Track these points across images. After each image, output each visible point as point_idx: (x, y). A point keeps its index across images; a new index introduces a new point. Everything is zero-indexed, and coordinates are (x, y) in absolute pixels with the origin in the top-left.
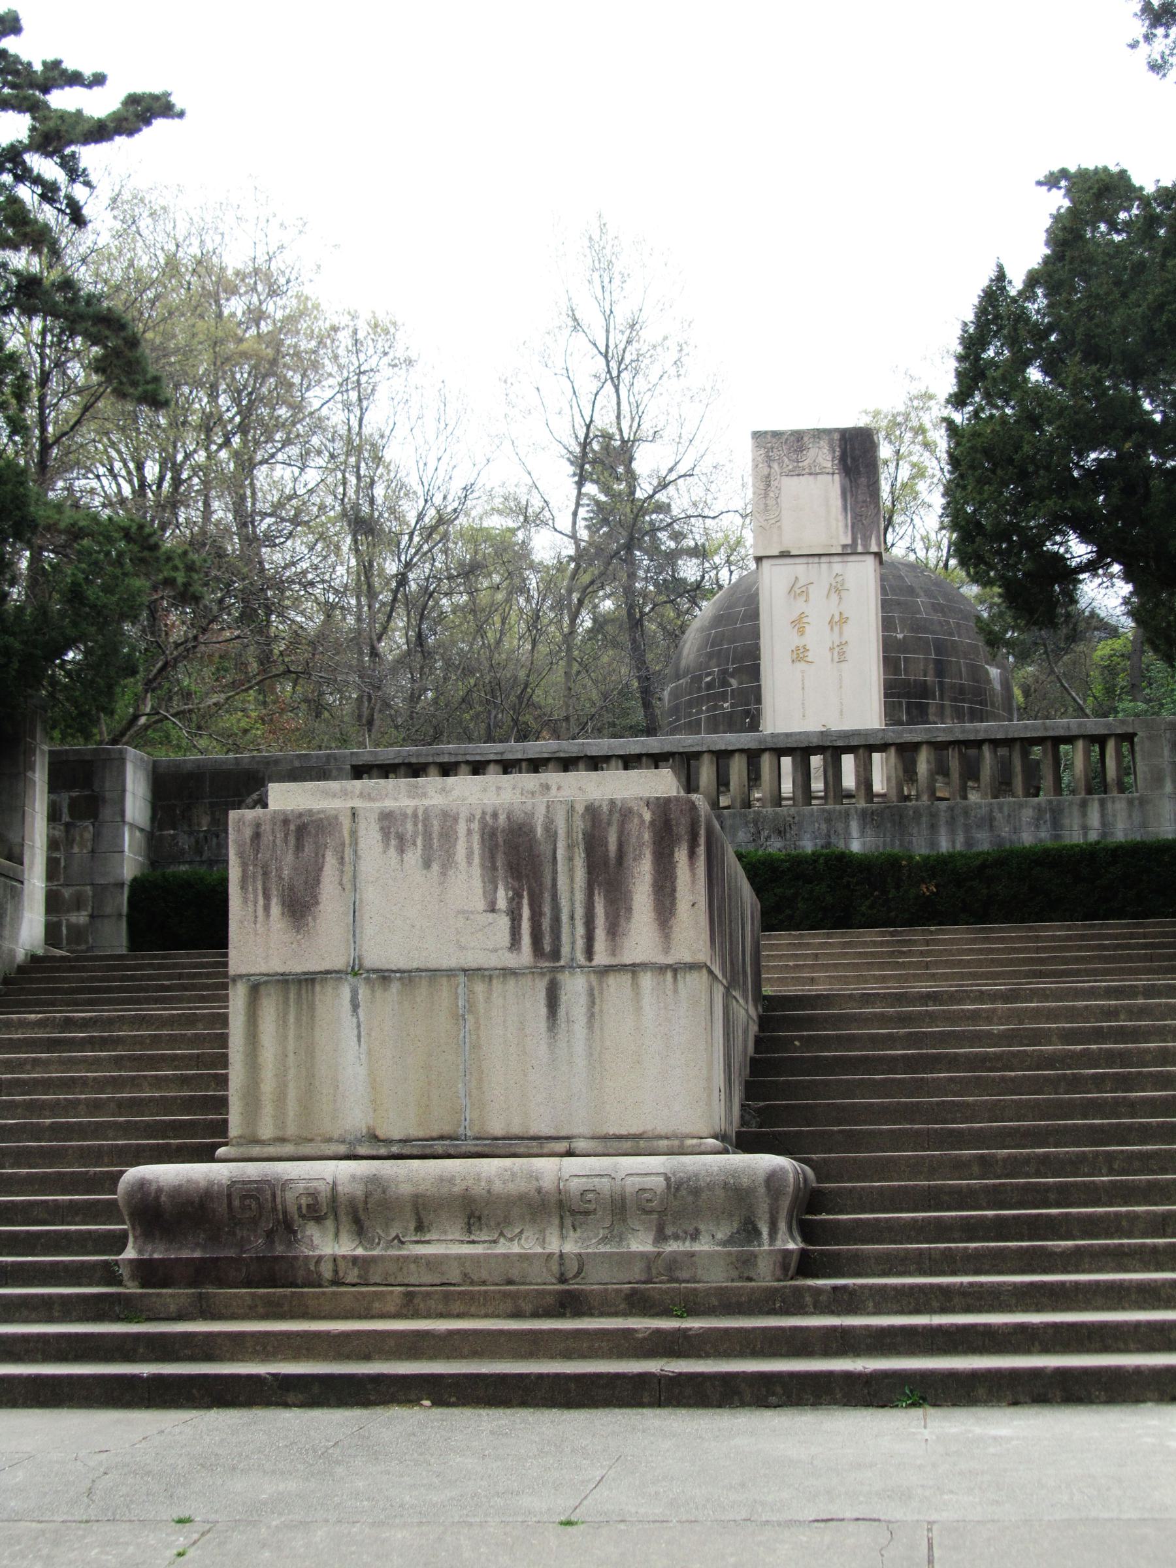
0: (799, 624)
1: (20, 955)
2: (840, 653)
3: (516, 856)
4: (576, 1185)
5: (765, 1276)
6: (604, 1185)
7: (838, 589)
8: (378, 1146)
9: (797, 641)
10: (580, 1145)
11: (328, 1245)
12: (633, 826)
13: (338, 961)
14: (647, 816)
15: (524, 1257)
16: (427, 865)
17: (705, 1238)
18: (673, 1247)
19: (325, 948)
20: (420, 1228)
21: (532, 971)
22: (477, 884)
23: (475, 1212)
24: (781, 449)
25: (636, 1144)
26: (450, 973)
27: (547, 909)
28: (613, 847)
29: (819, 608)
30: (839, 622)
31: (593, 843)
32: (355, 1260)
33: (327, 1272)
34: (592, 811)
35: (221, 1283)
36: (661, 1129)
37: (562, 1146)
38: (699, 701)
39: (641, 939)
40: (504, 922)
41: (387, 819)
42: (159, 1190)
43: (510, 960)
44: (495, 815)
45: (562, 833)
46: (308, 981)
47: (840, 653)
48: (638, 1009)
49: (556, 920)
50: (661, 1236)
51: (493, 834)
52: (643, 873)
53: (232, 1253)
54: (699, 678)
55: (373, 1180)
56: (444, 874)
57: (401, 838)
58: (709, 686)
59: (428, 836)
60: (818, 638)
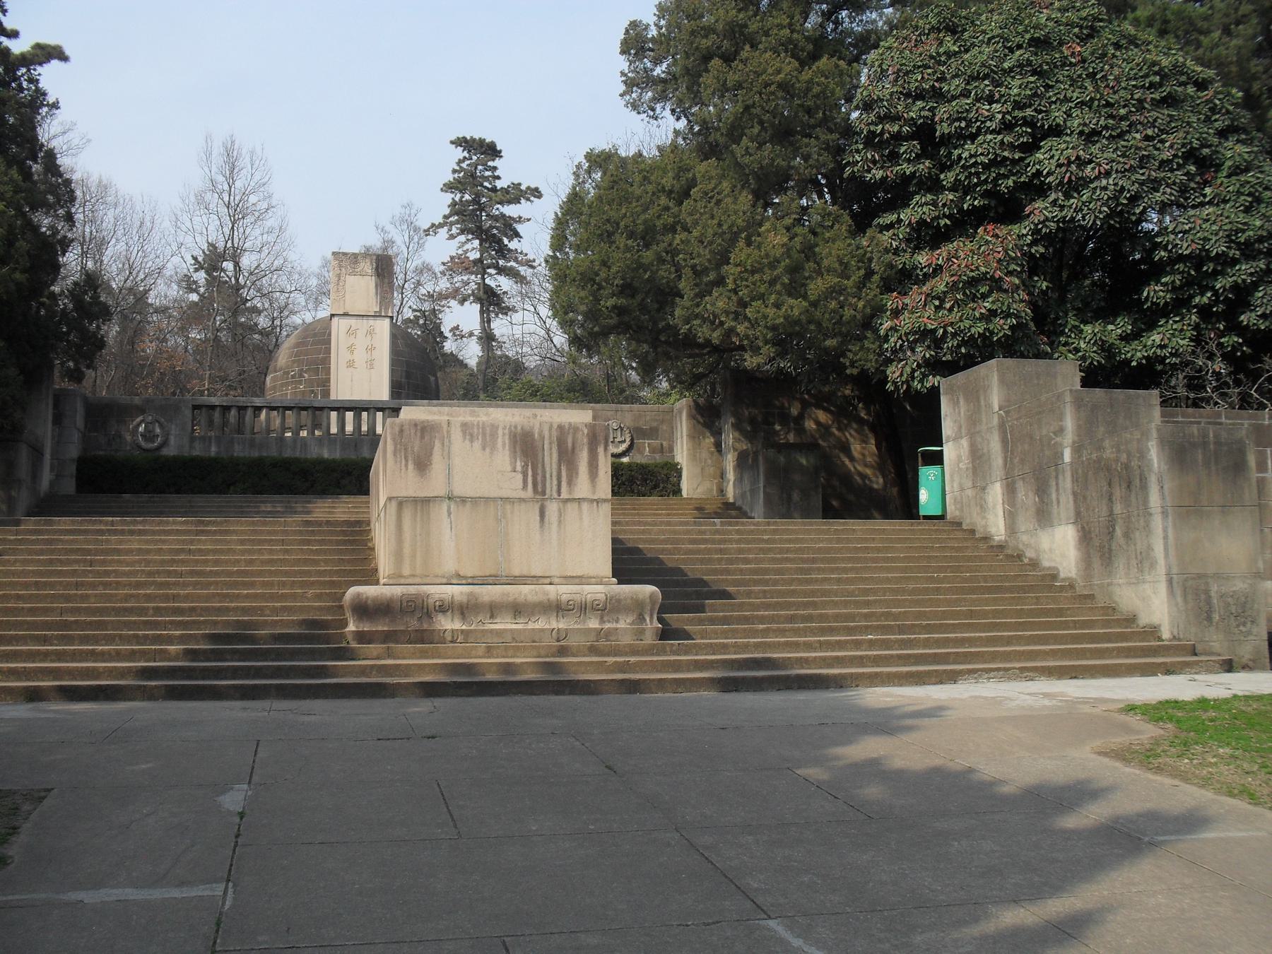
0: (351, 349)
1: (42, 495)
2: (371, 364)
3: (525, 446)
4: (564, 598)
5: (649, 639)
6: (577, 598)
7: (371, 332)
8: (459, 579)
9: (350, 357)
10: (556, 580)
11: (448, 624)
12: (579, 435)
13: (442, 493)
14: (586, 431)
15: (542, 630)
16: (484, 449)
17: (622, 622)
18: (607, 626)
19: (435, 485)
20: (492, 617)
21: (532, 500)
22: (507, 459)
23: (518, 609)
24: (346, 260)
25: (581, 580)
26: (494, 499)
27: (540, 472)
28: (570, 445)
29: (361, 342)
30: (370, 349)
31: (561, 443)
32: (462, 631)
33: (448, 637)
34: (560, 427)
35: (397, 643)
36: (591, 574)
37: (548, 581)
38: (287, 384)
39: (583, 487)
40: (520, 476)
41: (465, 427)
42: (367, 598)
43: (522, 495)
44: (516, 427)
45: (547, 437)
46: (426, 501)
47: (371, 364)
48: (581, 519)
49: (544, 477)
50: (602, 621)
51: (515, 436)
52: (584, 456)
53: (402, 628)
54: (288, 373)
55: (471, 594)
56: (491, 453)
57: (471, 435)
58: (293, 377)
59: (484, 434)
60: (360, 356)
